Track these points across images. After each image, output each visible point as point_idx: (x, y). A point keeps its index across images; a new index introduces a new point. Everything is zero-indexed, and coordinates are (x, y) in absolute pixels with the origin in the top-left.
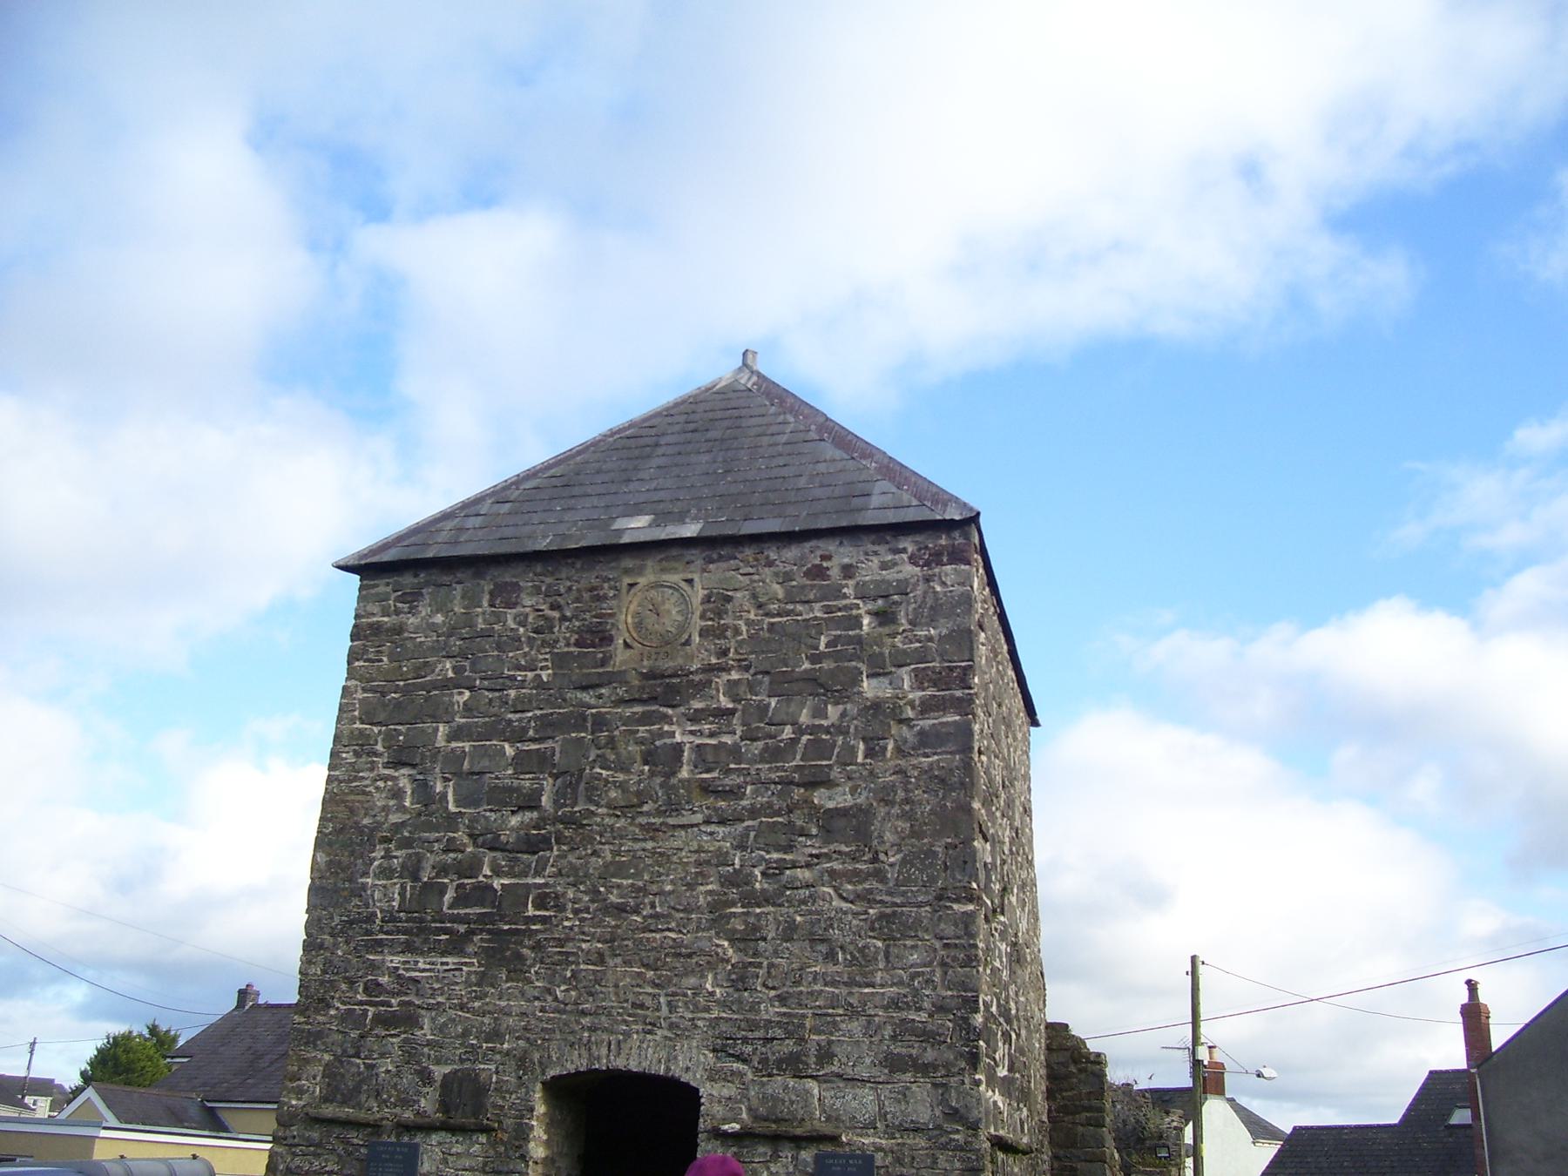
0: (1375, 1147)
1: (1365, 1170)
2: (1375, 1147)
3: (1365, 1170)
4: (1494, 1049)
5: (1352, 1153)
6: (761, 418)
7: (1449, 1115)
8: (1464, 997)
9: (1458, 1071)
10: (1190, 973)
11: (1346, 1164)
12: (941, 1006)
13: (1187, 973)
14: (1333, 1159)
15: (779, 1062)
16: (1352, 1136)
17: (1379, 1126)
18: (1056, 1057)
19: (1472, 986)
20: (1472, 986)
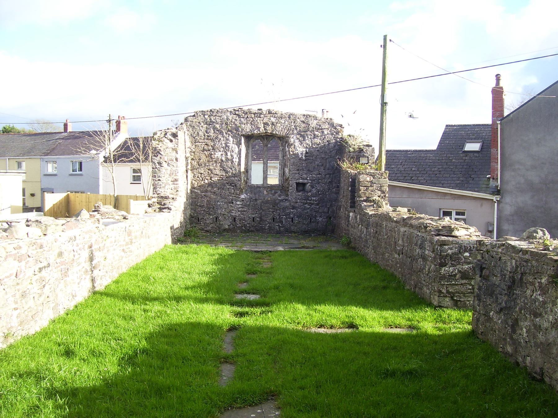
0: (427, 161)
1: (425, 172)
2: (427, 161)
3: (425, 172)
4: (506, 114)
5: (416, 164)
6: (188, 177)
7: (463, 146)
8: (494, 84)
9: (488, 125)
10: (383, 46)
11: (413, 169)
12: (132, 242)
13: (381, 47)
14: (405, 166)
15: (188, 162)
16: (413, 155)
17: (426, 151)
18: (52, 216)
19: (498, 77)
20: (498, 77)
